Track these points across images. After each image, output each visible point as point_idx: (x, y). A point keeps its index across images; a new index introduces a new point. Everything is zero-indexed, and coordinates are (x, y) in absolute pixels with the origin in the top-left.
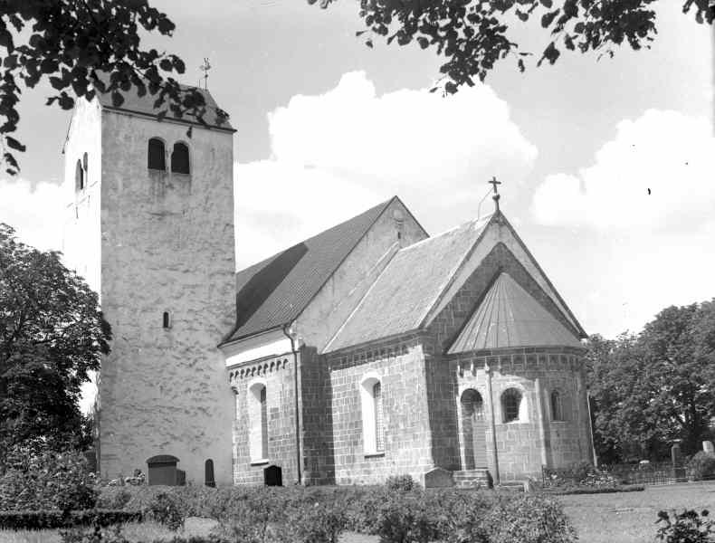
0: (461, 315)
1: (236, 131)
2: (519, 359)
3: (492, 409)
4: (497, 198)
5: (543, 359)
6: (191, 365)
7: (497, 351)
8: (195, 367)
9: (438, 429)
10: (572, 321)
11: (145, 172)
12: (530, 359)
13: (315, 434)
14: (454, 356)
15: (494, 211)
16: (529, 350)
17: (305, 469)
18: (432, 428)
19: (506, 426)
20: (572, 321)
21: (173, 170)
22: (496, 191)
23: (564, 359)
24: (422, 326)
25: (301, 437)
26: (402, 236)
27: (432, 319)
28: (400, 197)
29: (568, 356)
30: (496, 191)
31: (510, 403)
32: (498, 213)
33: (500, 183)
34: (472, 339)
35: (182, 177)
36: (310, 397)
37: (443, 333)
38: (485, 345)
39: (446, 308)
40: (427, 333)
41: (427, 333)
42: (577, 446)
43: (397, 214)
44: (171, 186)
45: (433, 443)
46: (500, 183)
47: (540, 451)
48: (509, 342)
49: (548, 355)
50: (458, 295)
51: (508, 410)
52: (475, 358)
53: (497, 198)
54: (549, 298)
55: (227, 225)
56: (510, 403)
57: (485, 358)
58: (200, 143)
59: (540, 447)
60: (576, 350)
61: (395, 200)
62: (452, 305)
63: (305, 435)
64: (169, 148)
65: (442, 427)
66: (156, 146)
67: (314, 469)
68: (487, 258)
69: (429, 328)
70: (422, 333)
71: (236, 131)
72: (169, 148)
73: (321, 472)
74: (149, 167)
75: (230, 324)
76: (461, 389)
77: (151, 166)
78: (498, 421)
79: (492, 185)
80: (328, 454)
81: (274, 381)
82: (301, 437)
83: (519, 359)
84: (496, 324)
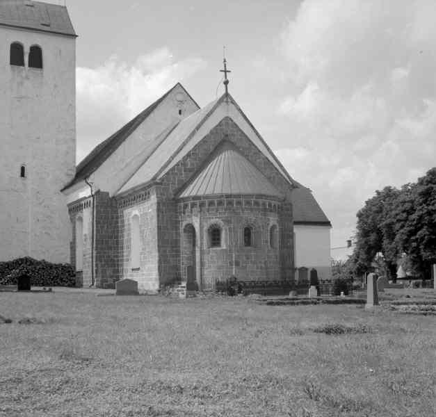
0: (190, 170)
1: (77, 36)
2: (220, 203)
3: (203, 239)
4: (226, 83)
5: (248, 203)
6: (40, 204)
7: (206, 197)
8: (43, 204)
9: (165, 251)
10: (286, 177)
11: (8, 66)
12: (230, 203)
13: (105, 253)
14: (184, 199)
15: (224, 92)
16: (228, 196)
17: (96, 277)
18: (159, 251)
19: (209, 251)
20: (284, 174)
21: (30, 66)
22: (226, 78)
23: (257, 203)
24: (154, 179)
25: (94, 255)
26: (182, 113)
27: (163, 173)
28: (181, 83)
29: (261, 201)
30: (226, 78)
31: (215, 235)
32: (227, 95)
33: (229, 72)
34: (201, 187)
35: (37, 71)
36: (102, 227)
37: (174, 184)
38: (214, 191)
39: (177, 165)
40: (161, 184)
41: (161, 184)
42: (263, 265)
43: (180, 97)
44: (27, 78)
45: (160, 262)
46: (229, 72)
47: (232, 268)
48: (231, 190)
49: (243, 200)
50: (188, 155)
51: (214, 239)
52: (192, 201)
53: (226, 83)
54: (267, 158)
55: (71, 105)
56: (215, 235)
57: (202, 203)
58: (49, 46)
59: (232, 265)
60: (268, 196)
61: (179, 83)
62: (183, 163)
63: (97, 253)
64: (27, 50)
65: (168, 249)
66: (16, 50)
67: (103, 277)
68: (215, 128)
69: (162, 179)
70: (157, 184)
71: (77, 36)
72: (27, 50)
73: (109, 279)
74: (11, 64)
75: (72, 175)
76: (184, 224)
77: (13, 62)
78: (205, 248)
79: (223, 73)
80: (115, 267)
81: (144, 208)
82: (94, 255)
83: (220, 203)
84: (215, 179)
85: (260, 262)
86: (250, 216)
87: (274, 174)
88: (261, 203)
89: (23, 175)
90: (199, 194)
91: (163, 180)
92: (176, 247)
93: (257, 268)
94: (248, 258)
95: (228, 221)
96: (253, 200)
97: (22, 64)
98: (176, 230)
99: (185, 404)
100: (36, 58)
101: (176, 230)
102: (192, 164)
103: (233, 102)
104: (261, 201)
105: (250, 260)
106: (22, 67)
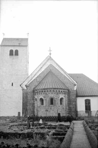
13: (24, 107)
21: (15, 55)
32: (50, 57)
50: (38, 77)
64: (14, 51)
67: (25, 114)
72: (14, 51)
74: (10, 55)
85: (56, 110)
86: (51, 95)
87: (68, 81)
88: (60, 91)
89: (12, 85)
90: (45, 88)
91: (29, 85)
92: (34, 105)
93: (54, 112)
94: (51, 109)
95: (64, 97)
96: (52, 90)
97: (13, 55)
98: (34, 100)
99: (13, 142)
100: (17, 53)
101: (34, 100)
102: (39, 80)
103: (52, 60)
104: (55, 90)
105: (51, 110)
106: (13, 56)
